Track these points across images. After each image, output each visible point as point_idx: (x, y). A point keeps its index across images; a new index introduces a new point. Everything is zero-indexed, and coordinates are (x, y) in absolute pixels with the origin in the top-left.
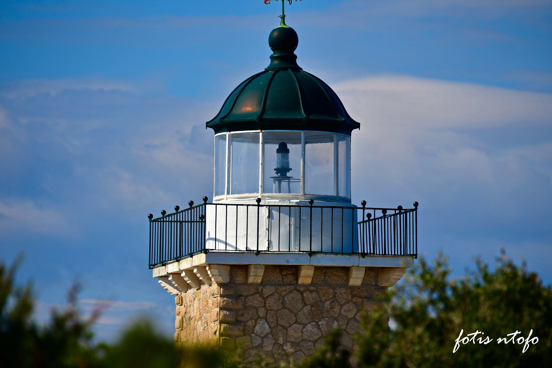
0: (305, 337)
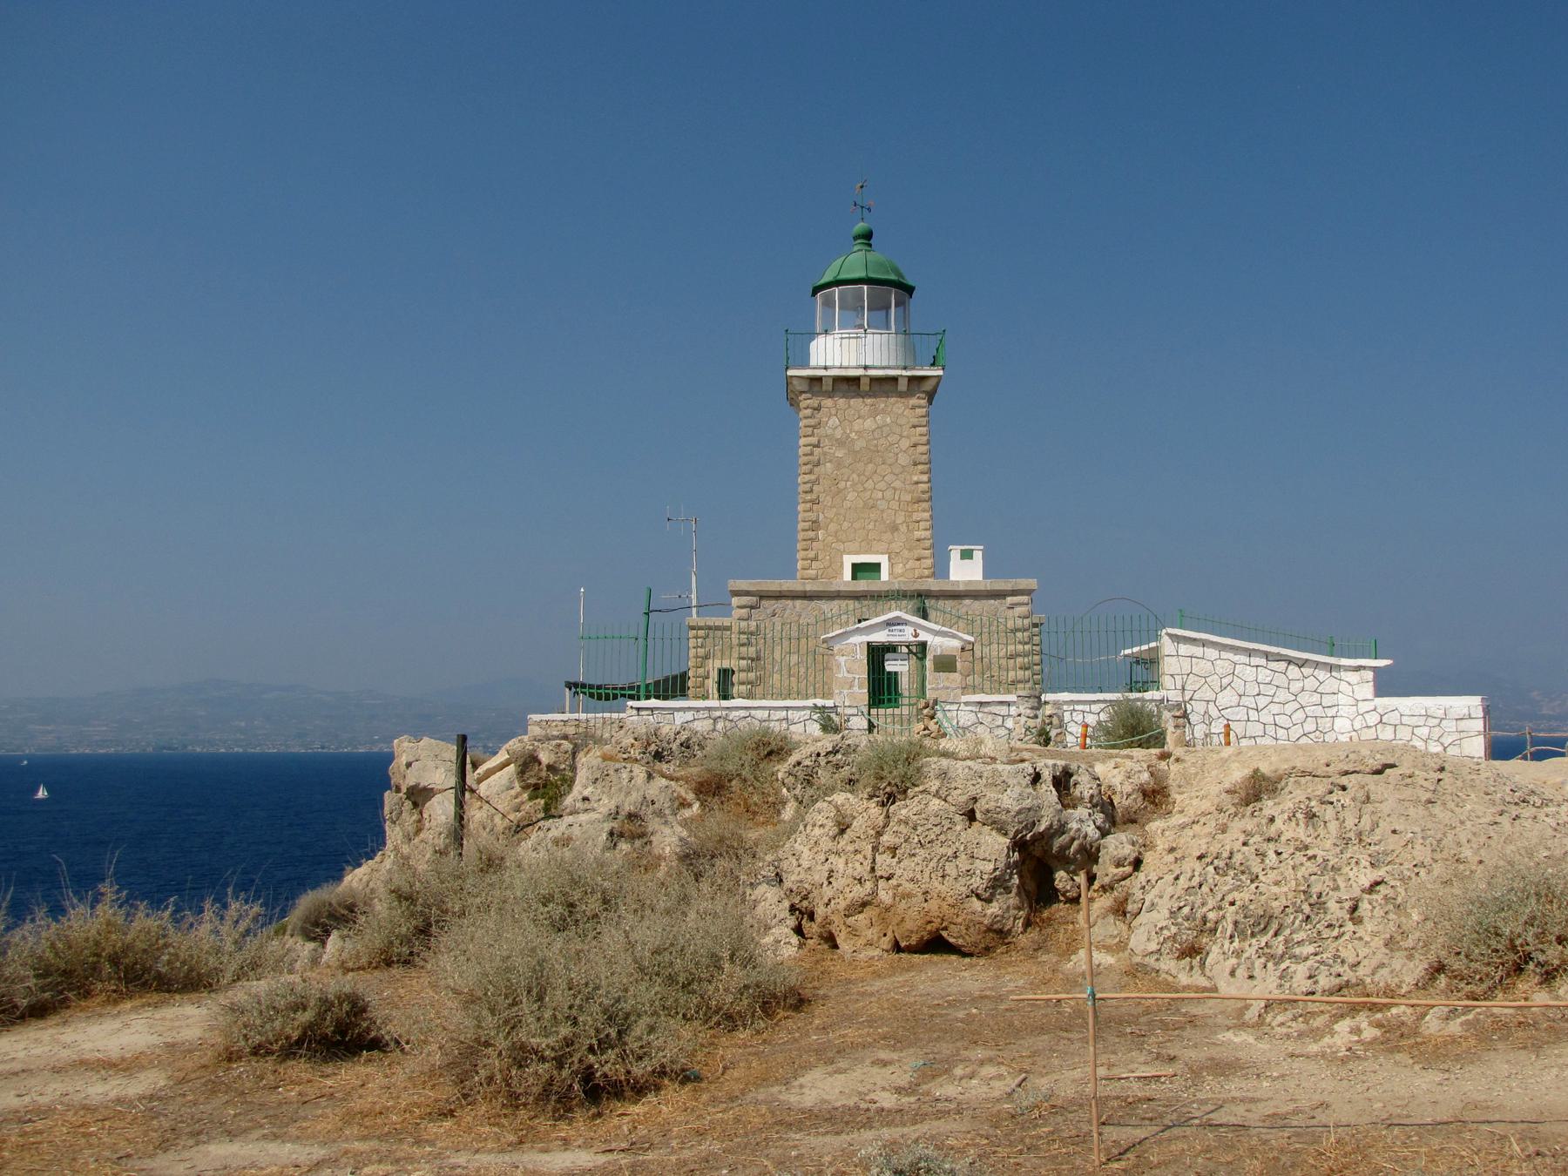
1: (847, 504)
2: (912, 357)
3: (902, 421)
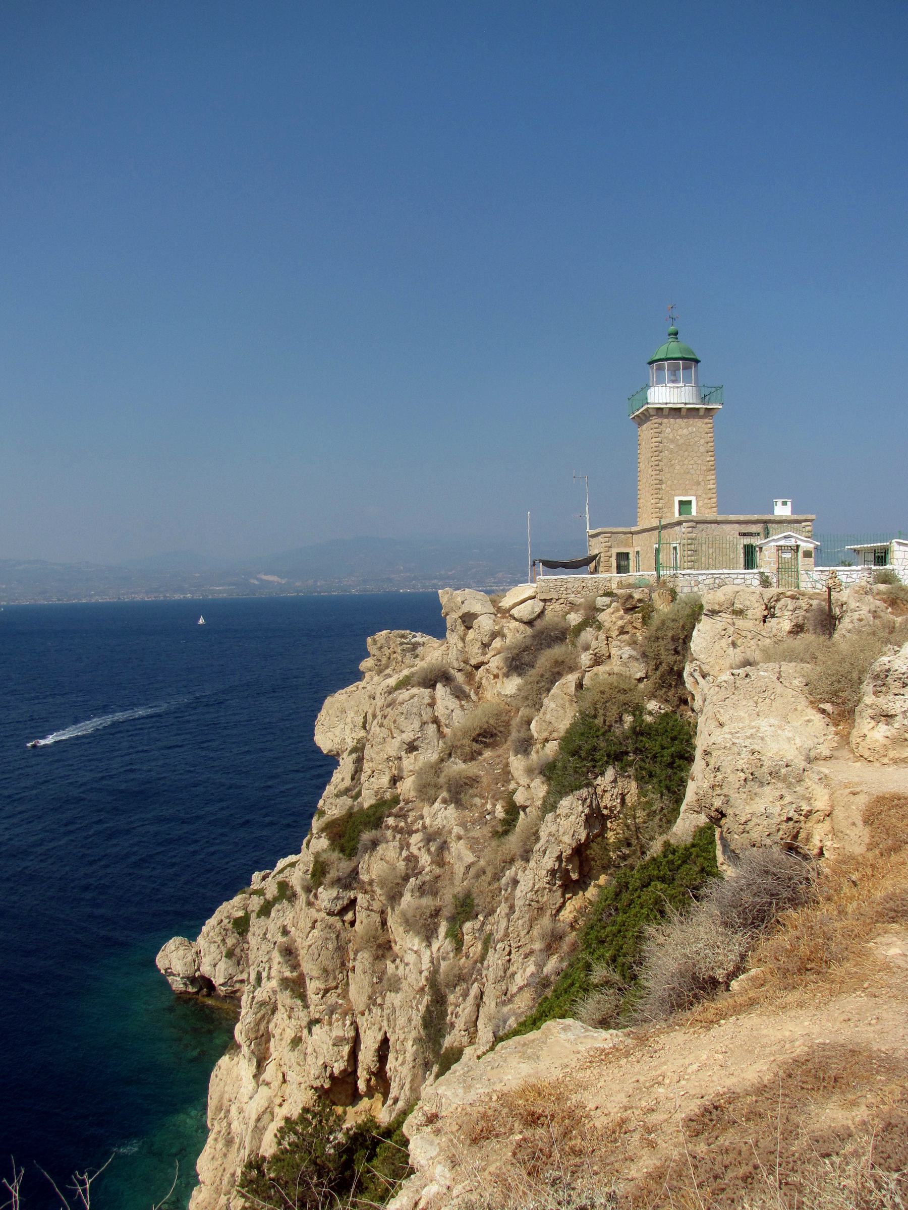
1: (676, 471)
2: (704, 399)
3: (701, 430)
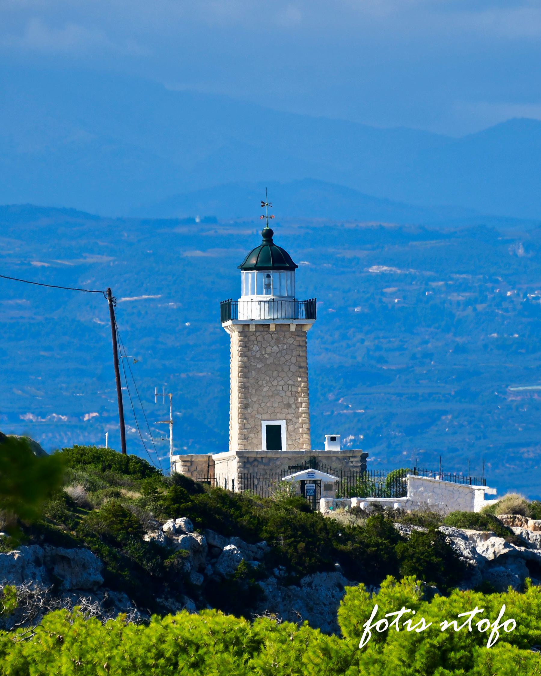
0: (273, 351)
1: (263, 393)
